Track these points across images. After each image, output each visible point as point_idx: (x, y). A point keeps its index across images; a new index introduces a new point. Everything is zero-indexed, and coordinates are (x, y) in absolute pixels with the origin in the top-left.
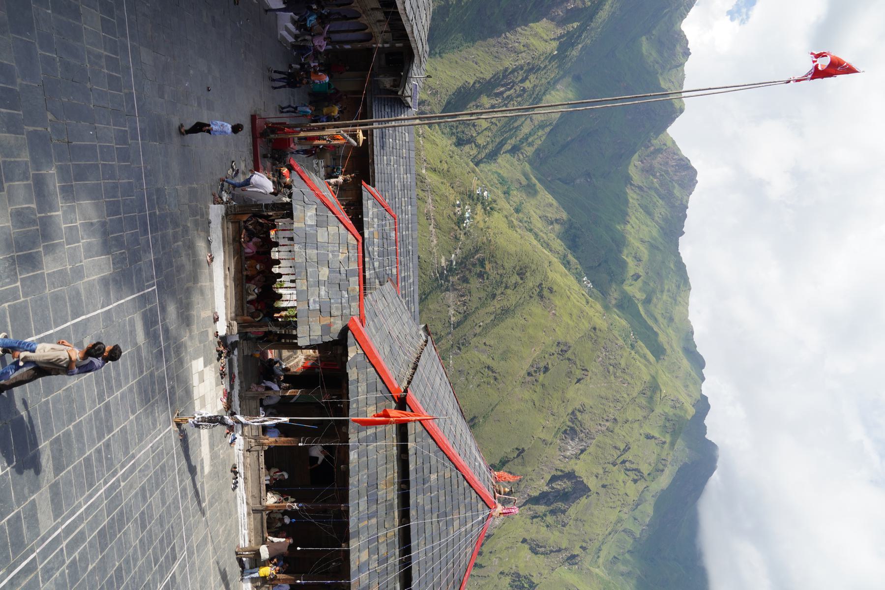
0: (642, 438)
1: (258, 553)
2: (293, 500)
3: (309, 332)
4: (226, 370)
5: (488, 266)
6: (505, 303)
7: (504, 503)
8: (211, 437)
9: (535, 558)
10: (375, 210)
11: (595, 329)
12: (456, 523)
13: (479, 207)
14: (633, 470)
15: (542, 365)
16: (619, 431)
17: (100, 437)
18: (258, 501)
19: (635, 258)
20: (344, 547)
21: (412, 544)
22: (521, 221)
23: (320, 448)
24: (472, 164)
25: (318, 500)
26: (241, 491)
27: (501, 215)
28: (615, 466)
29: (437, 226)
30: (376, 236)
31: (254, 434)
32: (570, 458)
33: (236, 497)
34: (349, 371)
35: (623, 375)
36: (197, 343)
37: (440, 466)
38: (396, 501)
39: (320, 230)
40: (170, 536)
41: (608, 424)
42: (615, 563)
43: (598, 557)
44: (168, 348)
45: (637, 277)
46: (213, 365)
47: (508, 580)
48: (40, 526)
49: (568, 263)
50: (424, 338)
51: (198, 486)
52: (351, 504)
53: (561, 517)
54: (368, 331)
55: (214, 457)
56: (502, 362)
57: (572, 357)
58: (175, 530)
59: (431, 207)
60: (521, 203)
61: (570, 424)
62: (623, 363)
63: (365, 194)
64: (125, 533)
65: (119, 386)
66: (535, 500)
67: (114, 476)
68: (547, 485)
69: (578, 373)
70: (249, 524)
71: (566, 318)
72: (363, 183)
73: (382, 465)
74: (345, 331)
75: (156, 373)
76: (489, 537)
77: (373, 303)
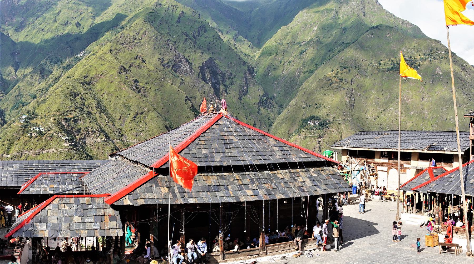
2: (217, 237)
3: (115, 229)
5: (70, 116)
6: (93, 106)
10: (36, 186)
11: (111, 50)
12: (231, 137)
13: (32, 121)
14: (199, 31)
15: (133, 84)
19: (65, 25)
20: (244, 205)
21: (243, 164)
22: (42, 96)
24: (5, 126)
25: (218, 222)
27: (38, 108)
28: (196, 42)
29: (44, 149)
30: (52, 186)
34: (139, 204)
35: (140, 35)
37: (198, 147)
39: (50, 221)
41: (171, 45)
43: (249, 56)
45: (78, 24)
47: (262, 109)
49: (68, 66)
53: (226, 76)
54: (114, 191)
56: (131, 108)
57: (128, 65)
59: (32, 152)
60: (30, 95)
61: (170, 68)
62: (132, 34)
63: (26, 192)
69: (139, 61)
71: (104, 68)
72: (18, 193)
73: (197, 183)
74: (113, 206)
77: (95, 189)
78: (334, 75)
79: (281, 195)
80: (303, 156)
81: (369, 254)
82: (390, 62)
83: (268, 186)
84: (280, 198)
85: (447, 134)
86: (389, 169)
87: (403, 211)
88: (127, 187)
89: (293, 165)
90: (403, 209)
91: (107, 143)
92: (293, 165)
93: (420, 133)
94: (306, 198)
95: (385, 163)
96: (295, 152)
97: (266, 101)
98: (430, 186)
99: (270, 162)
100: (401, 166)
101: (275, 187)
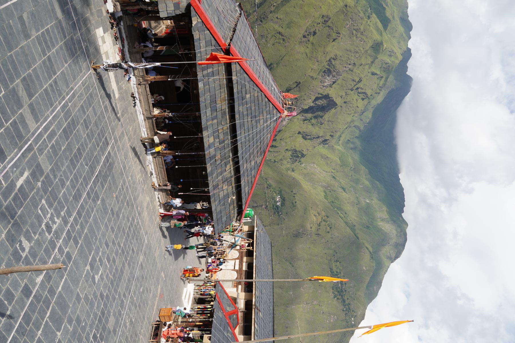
0: (370, 74)
1: (153, 140)
2: (169, 111)
4: (118, 35)
7: (290, 109)
8: (116, 77)
9: (305, 141)
11: (346, 6)
12: (262, 121)
14: (362, 93)
15: (312, 30)
16: (356, 71)
17: (50, 77)
18: (149, 113)
23: (181, 81)
26: (138, 107)
31: (141, 74)
32: (326, 87)
33: (136, 111)
34: (193, 33)
35: (361, 36)
36: (96, 17)
37: (251, 90)
38: (227, 110)
40: (102, 133)
41: (350, 66)
42: (348, 143)
44: (78, 20)
46: (109, 32)
47: (290, 153)
48: (29, 127)
50: (239, 12)
51: (114, 105)
52: (202, 112)
53: (320, 120)
54: (204, 7)
55: (120, 88)
57: (331, 25)
58: (105, 129)
61: (328, 67)
62: (362, 28)
64: (77, 131)
65: (54, 46)
66: (306, 111)
67: (64, 100)
68: (313, 102)
69: (334, 35)
70: (146, 125)
73: (218, 90)
74: (189, 6)
75: (74, 38)
76: (280, 131)
78: (324, 218)
79: (210, 169)
80: (247, 188)
81: (155, 252)
82: (339, 271)
83: (218, 157)
84: (208, 168)
85: (271, 328)
86: (237, 271)
87: (196, 285)
88: (209, 20)
89: (238, 180)
90: (198, 286)
91: (253, 6)
92: (238, 180)
93: (271, 300)
94: (208, 192)
95: (242, 267)
96: (250, 181)
97: (298, 157)
98: (219, 312)
99: (240, 158)
100: (240, 283)
101: (217, 163)
